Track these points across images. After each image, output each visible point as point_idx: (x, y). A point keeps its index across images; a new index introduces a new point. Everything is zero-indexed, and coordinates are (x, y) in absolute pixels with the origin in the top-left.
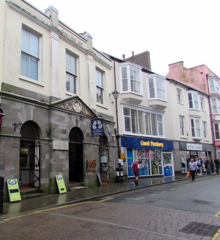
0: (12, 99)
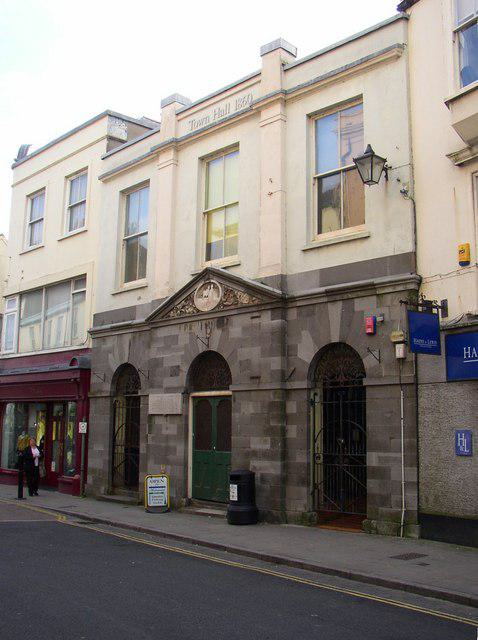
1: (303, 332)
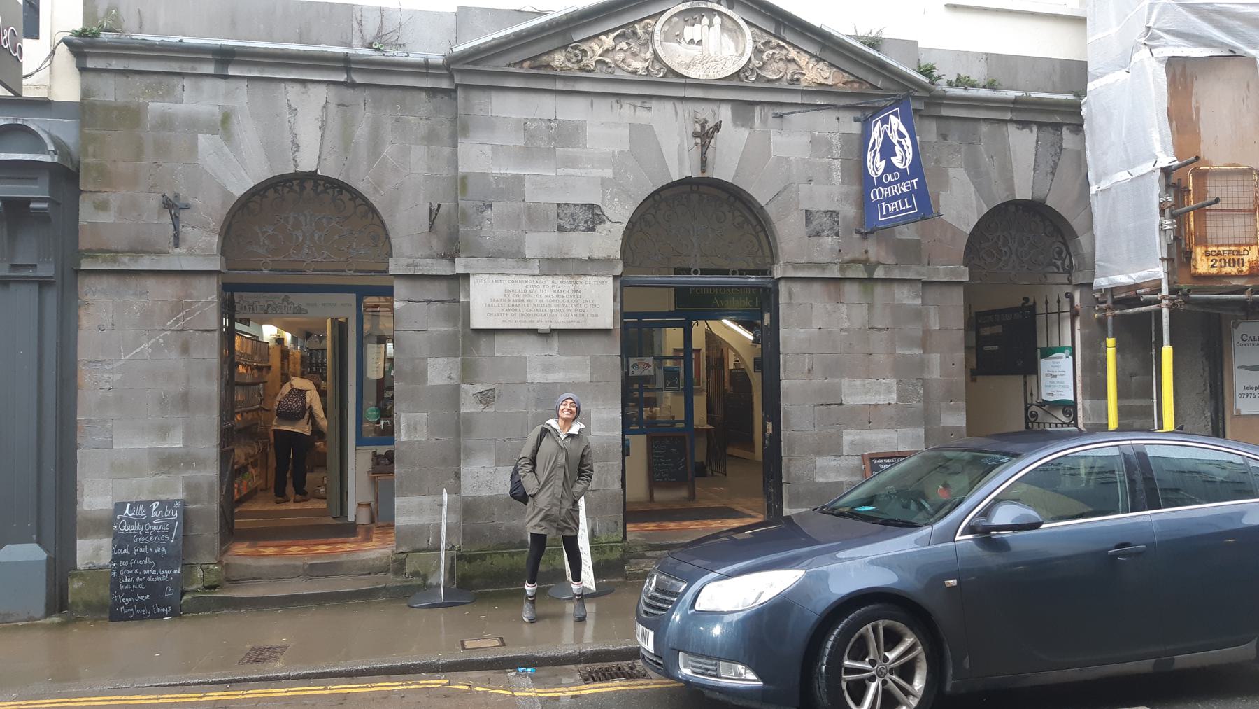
0: (115, 64)
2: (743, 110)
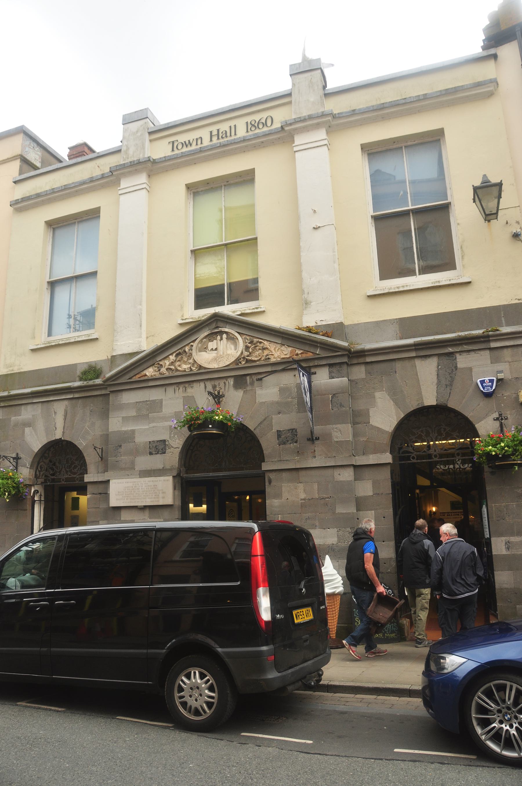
1: (378, 395)
2: (240, 382)
